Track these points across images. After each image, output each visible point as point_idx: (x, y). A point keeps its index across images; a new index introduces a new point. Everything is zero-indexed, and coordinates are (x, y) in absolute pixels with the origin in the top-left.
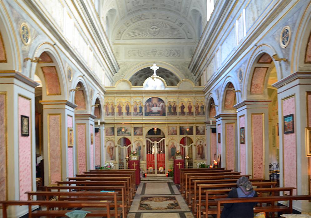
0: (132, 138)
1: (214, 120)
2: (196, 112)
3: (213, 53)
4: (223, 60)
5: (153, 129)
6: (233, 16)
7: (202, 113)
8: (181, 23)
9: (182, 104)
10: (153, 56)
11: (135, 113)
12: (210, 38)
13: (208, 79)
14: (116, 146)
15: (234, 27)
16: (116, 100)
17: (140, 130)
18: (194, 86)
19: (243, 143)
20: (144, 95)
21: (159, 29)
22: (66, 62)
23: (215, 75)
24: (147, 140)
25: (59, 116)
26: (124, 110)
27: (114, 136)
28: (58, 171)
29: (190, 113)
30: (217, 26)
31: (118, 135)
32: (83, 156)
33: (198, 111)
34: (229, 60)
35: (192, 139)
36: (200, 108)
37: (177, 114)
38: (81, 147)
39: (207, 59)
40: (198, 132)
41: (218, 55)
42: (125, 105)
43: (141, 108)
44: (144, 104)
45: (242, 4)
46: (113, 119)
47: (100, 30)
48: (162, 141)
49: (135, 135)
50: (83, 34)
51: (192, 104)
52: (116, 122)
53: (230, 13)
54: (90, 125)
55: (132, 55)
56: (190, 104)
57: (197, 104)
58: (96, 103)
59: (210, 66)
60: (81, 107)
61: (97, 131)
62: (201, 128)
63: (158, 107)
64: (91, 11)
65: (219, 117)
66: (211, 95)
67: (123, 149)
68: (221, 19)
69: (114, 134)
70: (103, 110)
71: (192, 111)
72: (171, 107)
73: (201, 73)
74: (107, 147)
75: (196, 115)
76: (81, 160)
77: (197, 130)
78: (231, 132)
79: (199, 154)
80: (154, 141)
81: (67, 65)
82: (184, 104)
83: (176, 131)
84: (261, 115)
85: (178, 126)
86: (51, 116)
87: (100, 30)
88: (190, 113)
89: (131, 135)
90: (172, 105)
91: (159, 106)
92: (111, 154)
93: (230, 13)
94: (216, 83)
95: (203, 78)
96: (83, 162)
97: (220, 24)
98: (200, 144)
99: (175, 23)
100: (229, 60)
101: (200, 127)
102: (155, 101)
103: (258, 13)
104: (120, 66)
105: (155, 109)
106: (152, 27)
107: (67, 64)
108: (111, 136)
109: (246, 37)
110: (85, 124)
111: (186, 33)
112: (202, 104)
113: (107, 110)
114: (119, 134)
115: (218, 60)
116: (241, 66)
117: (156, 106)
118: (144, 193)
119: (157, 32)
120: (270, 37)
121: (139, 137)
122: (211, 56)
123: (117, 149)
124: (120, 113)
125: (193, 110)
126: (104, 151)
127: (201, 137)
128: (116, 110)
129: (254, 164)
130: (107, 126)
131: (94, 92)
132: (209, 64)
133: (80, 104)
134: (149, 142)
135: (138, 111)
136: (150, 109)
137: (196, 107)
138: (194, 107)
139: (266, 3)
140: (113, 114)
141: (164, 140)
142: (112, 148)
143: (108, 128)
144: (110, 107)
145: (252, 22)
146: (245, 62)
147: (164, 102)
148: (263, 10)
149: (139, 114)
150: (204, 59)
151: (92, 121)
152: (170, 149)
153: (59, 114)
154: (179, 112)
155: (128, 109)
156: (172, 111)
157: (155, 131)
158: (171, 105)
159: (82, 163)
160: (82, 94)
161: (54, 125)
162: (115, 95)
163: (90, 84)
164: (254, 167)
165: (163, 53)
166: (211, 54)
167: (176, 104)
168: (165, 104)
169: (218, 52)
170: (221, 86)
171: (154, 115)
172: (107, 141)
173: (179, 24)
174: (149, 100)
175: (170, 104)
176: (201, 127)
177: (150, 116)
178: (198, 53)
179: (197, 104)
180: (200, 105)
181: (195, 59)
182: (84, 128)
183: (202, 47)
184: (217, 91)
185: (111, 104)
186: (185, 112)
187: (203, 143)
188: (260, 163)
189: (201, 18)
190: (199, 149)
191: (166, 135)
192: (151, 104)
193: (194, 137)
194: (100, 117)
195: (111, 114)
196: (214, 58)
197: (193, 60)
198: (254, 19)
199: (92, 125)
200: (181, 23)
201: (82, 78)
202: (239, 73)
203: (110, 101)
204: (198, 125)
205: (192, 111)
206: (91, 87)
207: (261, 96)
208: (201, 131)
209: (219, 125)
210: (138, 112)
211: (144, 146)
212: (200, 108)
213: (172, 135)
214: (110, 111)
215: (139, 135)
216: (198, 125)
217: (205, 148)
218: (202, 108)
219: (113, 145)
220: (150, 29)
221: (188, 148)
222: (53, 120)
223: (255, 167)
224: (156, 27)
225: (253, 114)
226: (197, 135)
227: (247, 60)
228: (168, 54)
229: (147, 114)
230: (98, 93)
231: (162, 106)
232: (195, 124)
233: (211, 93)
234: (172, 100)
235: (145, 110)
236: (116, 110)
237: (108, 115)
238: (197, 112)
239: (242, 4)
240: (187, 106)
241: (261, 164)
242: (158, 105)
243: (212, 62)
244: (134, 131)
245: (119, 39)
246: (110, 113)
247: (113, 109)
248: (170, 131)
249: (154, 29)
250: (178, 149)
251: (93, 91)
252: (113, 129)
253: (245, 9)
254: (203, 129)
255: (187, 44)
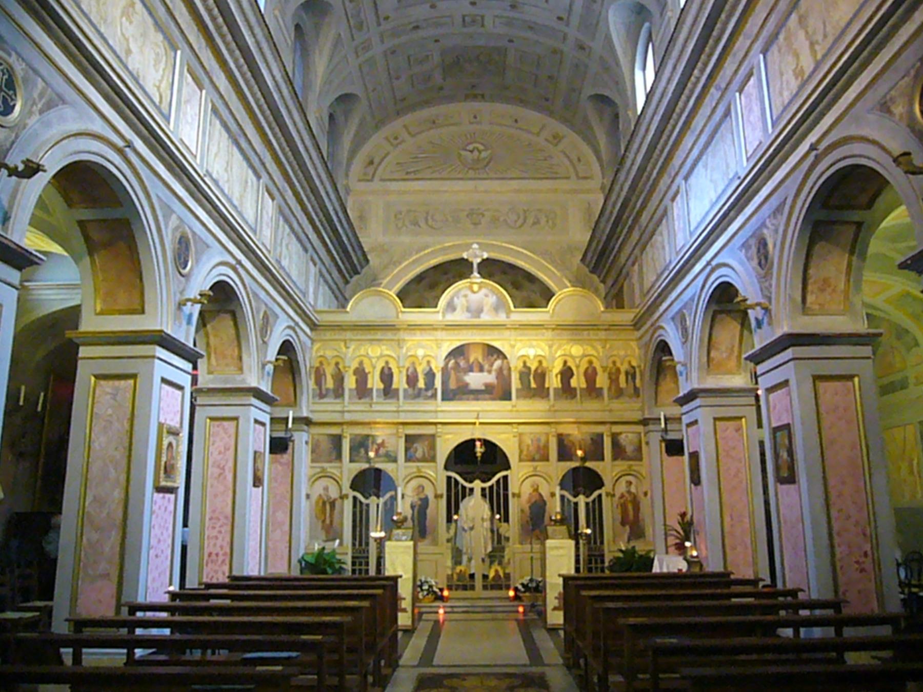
0: (397, 470)
1: (676, 410)
2: (609, 389)
3: (662, 207)
4: (693, 225)
5: (470, 443)
6: (723, 86)
7: (632, 391)
8: (555, 137)
9: (565, 362)
10: (472, 226)
11: (410, 391)
12: (649, 162)
13: (647, 285)
14: (343, 497)
15: (727, 113)
16: (351, 350)
17: (426, 443)
18: (602, 309)
19: (791, 479)
20: (439, 335)
21: (489, 152)
22: (169, 212)
23: (671, 268)
24: (449, 478)
25: (131, 382)
26: (375, 382)
27: (337, 464)
28: (107, 576)
29: (592, 391)
30: (672, 122)
31: (351, 461)
32: (221, 526)
33: (618, 384)
34: (719, 212)
35: (600, 473)
36: (622, 378)
37: (548, 395)
38: (216, 496)
39: (640, 227)
40: (619, 452)
41: (677, 209)
42: (381, 364)
43: (430, 375)
44: (441, 364)
45: (753, 43)
46: (338, 408)
47: (319, 176)
48: (498, 481)
49: (408, 459)
50: (244, 145)
51: (597, 364)
52: (348, 417)
53: (711, 77)
54: (252, 421)
55: (407, 223)
56: (590, 362)
57: (614, 363)
58: (279, 354)
59: (652, 246)
60: (227, 365)
61: (279, 446)
62: (628, 436)
63: (485, 374)
64: (273, 77)
65: (691, 396)
66: (660, 332)
67: (368, 505)
68: (683, 98)
69: (339, 457)
70: (308, 383)
71: (598, 386)
72: (529, 374)
73: (624, 271)
74: (314, 497)
75: (610, 398)
76: (217, 538)
77: (616, 444)
78: (734, 448)
79: (623, 523)
80: (471, 482)
81: (173, 221)
82: (571, 364)
83: (546, 447)
84: (850, 383)
85: (552, 430)
86: (102, 382)
87: (302, 140)
88: (592, 391)
89: (395, 460)
90: (533, 368)
91: (489, 372)
92: (328, 521)
93: (711, 77)
94: (674, 295)
95: (632, 286)
96: (222, 547)
97: (680, 116)
98: (629, 492)
99: (538, 134)
100: (719, 212)
101: (627, 436)
102: (476, 356)
103: (814, 52)
104: (369, 257)
105: (475, 380)
106: (471, 147)
107: (174, 217)
108: (330, 462)
109: (773, 137)
110: (236, 419)
111: (571, 161)
112: (630, 362)
113: (318, 382)
114: (356, 458)
115: (678, 225)
116: (763, 225)
117: (481, 370)
118: (432, 661)
119: (484, 159)
120: (872, 109)
121: (423, 467)
122: (652, 218)
123: (348, 505)
124: (363, 391)
125: (602, 381)
126: (304, 510)
127: (630, 467)
128: (350, 382)
129: (838, 556)
130: (315, 430)
131: (275, 322)
132: (651, 238)
133: (225, 357)
134: (457, 482)
135: (421, 384)
136: (459, 380)
137: (610, 374)
138: (604, 371)
139: (843, 13)
140: (338, 392)
141: (505, 478)
142: (333, 504)
143: (321, 438)
144: (329, 371)
145: (794, 84)
146: (778, 210)
147: (505, 357)
148: (830, 40)
149: (423, 393)
150: (631, 229)
151: (264, 411)
152: (526, 507)
153: (134, 376)
154: (555, 389)
155: (387, 376)
156: (533, 385)
157: (479, 449)
158: (529, 369)
159: (218, 550)
160: (231, 323)
161: (110, 411)
162: (349, 335)
163: (262, 295)
164: (838, 565)
165: (502, 219)
166: (652, 212)
167: (545, 364)
168: (508, 363)
169: (678, 198)
170: (692, 299)
171: (472, 396)
172: (314, 482)
173: (551, 139)
174: (458, 352)
175: (525, 363)
176: (630, 435)
177: (460, 399)
178: (611, 213)
179: (614, 363)
180: (624, 368)
181: (603, 232)
182: (232, 431)
183: (624, 194)
184: (678, 319)
185: (333, 362)
186: (575, 389)
187: (637, 489)
188: (862, 554)
189: (617, 116)
190: (624, 507)
191: (513, 459)
192: (462, 363)
193: (606, 468)
194: (294, 403)
195: (331, 394)
196: (664, 221)
197: (597, 235)
198: (798, 72)
199: (263, 424)
200: (555, 137)
201: (291, 332)
202: (754, 249)
203: (329, 353)
204: (616, 429)
205: (598, 386)
206: (266, 305)
207: (840, 318)
208: (629, 449)
209: (689, 425)
210: (420, 389)
211: (441, 496)
212: (622, 378)
213: (533, 460)
214: (330, 384)
215: (424, 460)
216: (616, 429)
217: (645, 503)
218: (631, 375)
219: (334, 493)
220: (463, 153)
221: (587, 504)
222: (108, 397)
223: (842, 567)
224: (481, 147)
225: (817, 378)
226: (617, 463)
227: (786, 199)
228: (519, 223)
229: (448, 396)
230: (289, 327)
231: (500, 370)
232: (608, 426)
233: (661, 327)
234: (531, 352)
235: (444, 383)
236: (350, 382)
237: (322, 396)
238: (613, 388)
239: (753, 43)
240: (582, 370)
241: (866, 554)
242: (486, 367)
243: (657, 232)
244: (407, 450)
245: (368, 181)
246: (327, 390)
247: (339, 379)
248: (525, 449)
249: (476, 153)
250: (555, 508)
251: (271, 320)
252: (337, 441)
253: (765, 52)
254: (636, 440)
255: (576, 192)
